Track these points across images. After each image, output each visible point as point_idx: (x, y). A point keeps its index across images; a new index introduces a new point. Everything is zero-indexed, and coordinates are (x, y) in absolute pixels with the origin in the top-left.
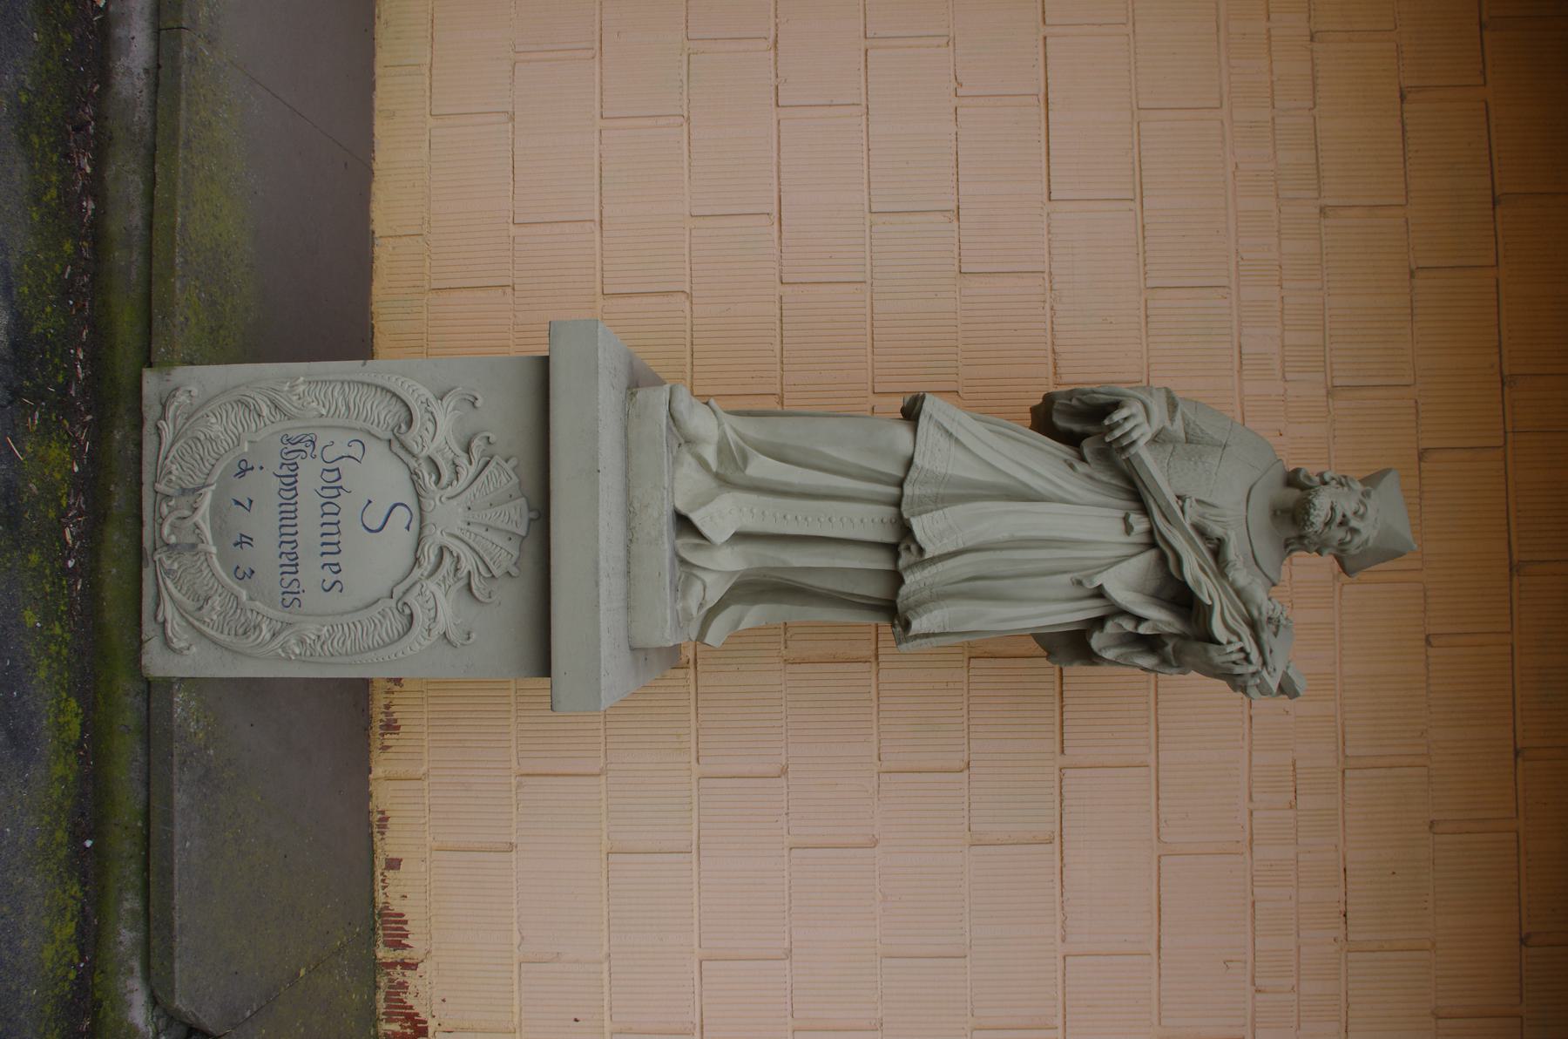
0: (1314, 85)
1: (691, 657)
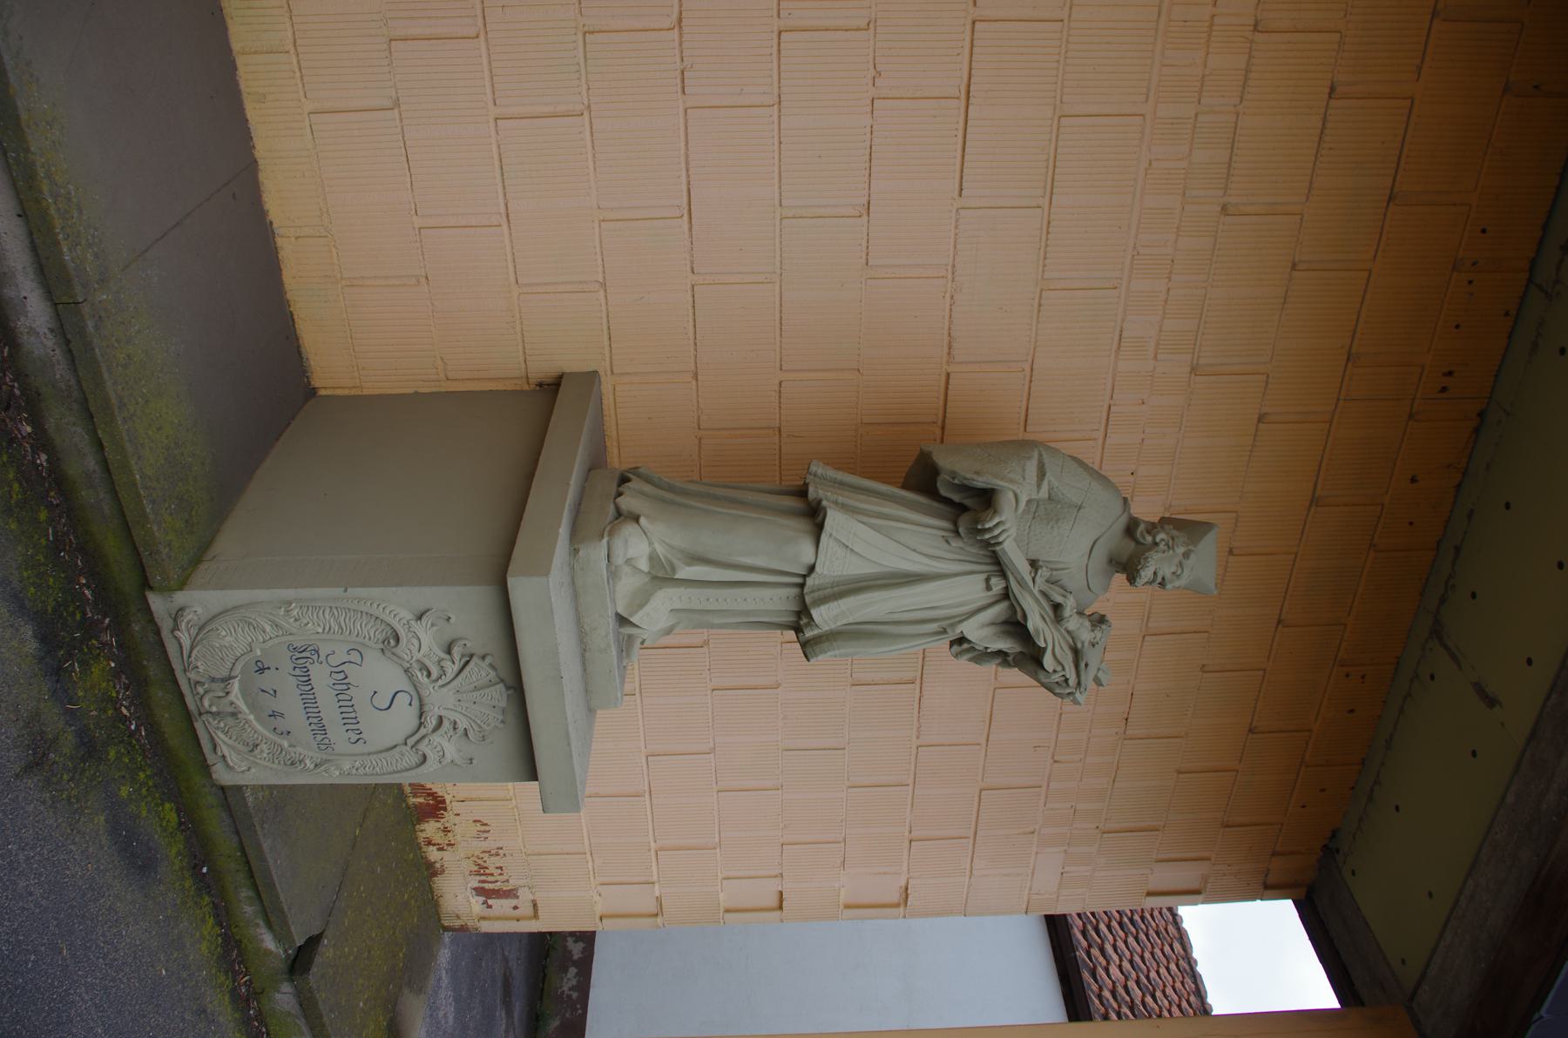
0: (1246, 78)
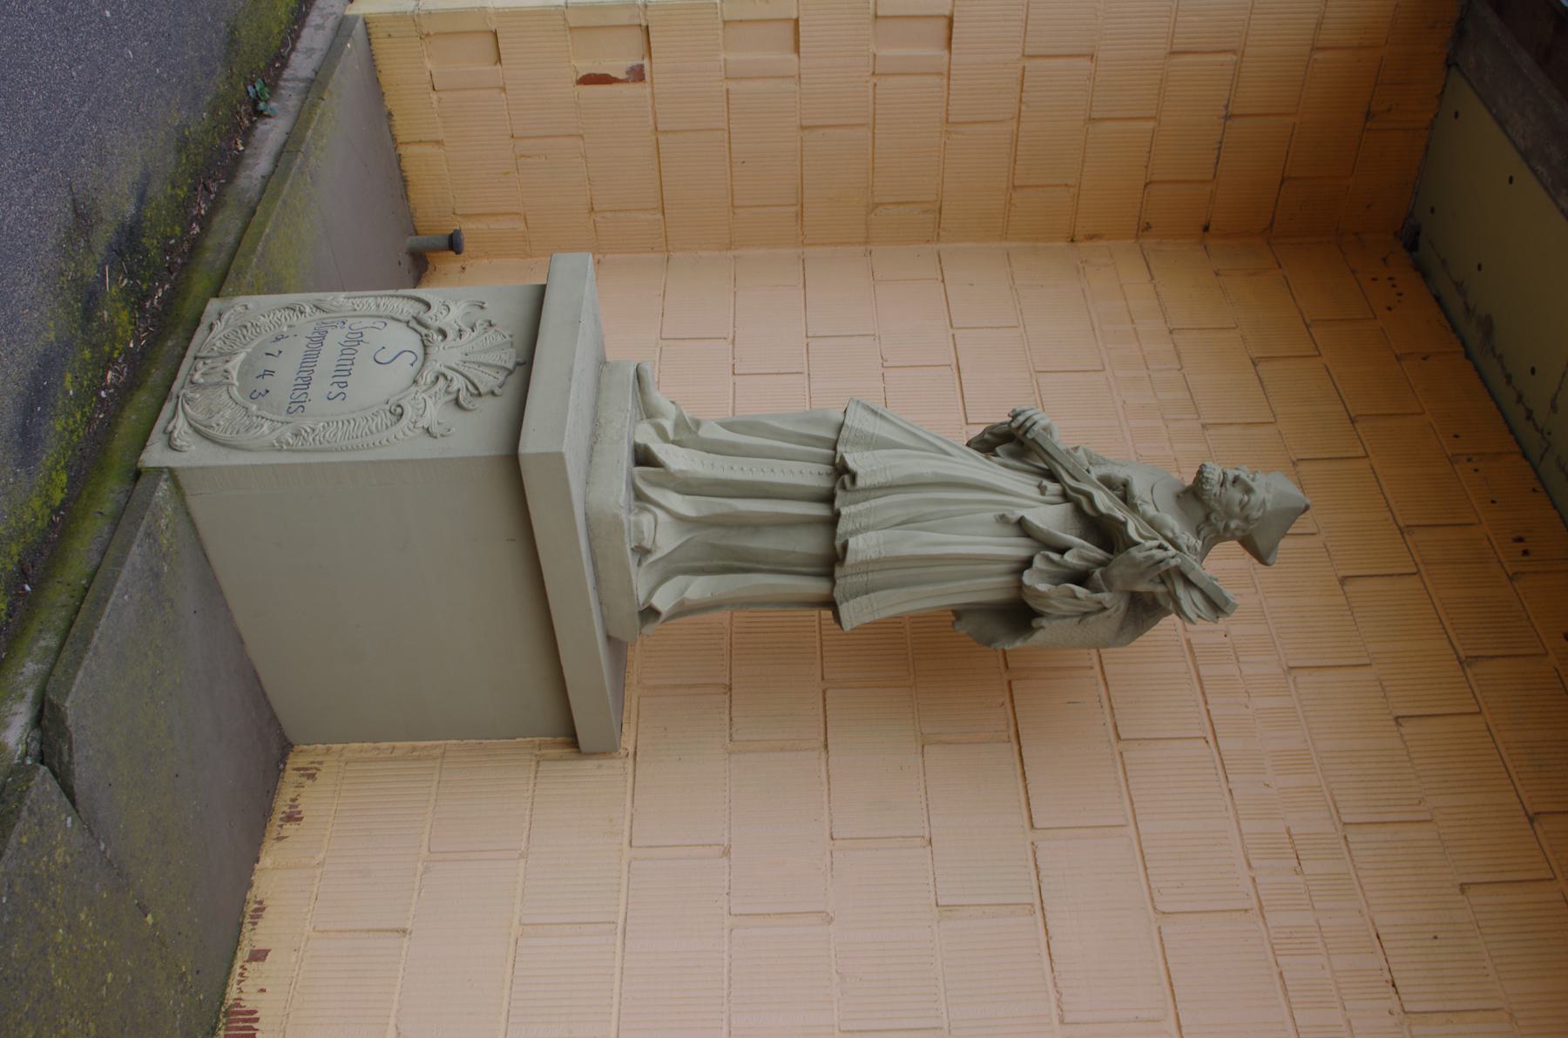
1: (631, 750)
